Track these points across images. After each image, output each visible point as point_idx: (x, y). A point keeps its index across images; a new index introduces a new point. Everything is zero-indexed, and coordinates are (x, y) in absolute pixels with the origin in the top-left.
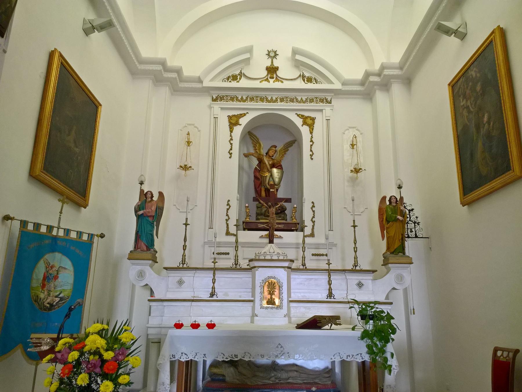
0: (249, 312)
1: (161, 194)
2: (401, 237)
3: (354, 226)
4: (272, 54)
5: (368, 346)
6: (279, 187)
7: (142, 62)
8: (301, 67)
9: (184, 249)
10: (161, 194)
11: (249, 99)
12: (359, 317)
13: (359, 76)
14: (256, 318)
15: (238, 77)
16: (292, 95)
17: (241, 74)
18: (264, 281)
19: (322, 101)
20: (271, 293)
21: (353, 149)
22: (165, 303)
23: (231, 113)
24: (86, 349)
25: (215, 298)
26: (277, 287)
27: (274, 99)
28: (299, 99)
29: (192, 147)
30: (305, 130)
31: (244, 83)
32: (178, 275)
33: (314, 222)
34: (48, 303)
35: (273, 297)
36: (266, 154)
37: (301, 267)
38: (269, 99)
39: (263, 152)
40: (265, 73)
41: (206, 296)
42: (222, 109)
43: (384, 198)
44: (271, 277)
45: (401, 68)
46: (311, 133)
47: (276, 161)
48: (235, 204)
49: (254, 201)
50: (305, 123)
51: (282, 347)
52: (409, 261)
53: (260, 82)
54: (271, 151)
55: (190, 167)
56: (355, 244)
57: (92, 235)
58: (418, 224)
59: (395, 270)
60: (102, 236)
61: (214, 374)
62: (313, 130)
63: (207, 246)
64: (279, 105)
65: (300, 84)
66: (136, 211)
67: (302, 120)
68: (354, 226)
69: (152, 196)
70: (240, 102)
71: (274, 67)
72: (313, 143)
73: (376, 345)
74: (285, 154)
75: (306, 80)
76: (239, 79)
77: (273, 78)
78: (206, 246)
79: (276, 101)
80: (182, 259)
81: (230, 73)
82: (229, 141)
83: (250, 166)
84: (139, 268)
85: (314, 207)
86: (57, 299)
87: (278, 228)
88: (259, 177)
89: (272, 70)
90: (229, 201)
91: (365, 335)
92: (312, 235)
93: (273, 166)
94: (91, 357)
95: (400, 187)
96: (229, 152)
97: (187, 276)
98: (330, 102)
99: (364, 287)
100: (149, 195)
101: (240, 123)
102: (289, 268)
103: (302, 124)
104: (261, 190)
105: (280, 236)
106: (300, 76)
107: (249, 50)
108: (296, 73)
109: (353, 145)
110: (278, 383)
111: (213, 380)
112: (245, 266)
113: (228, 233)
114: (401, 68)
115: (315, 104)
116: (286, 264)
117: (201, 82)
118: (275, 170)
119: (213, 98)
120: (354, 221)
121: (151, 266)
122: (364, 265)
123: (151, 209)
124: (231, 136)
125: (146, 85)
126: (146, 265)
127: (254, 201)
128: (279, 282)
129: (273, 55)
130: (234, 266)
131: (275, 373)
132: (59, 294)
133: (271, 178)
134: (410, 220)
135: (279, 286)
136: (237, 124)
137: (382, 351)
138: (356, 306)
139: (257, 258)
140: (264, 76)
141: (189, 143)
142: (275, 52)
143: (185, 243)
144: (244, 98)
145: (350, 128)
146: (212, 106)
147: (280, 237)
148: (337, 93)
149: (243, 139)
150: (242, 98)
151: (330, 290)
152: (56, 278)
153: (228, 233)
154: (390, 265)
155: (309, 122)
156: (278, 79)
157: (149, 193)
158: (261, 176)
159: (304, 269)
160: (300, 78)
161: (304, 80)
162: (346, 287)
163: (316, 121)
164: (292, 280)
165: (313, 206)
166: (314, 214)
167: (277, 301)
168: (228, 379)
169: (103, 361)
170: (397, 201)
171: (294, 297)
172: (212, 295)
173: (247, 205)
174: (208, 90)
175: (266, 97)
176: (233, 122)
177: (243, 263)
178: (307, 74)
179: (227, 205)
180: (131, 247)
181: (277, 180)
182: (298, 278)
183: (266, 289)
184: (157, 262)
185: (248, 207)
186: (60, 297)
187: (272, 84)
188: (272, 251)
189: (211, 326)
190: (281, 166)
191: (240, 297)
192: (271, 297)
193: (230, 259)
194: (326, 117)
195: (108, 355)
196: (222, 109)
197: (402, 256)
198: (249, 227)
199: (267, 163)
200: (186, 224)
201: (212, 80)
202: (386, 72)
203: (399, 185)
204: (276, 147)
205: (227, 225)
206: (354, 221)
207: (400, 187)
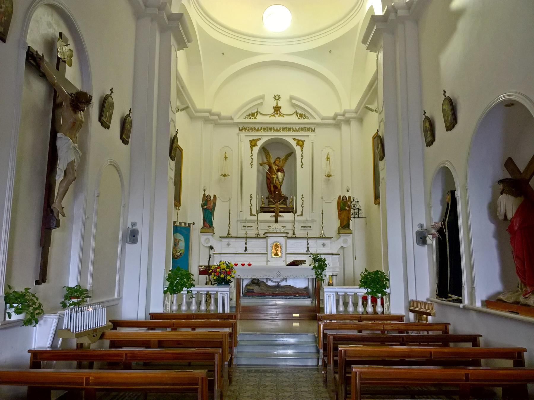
0: (265, 259)
1: (215, 196)
2: (347, 219)
3: (322, 213)
4: (277, 98)
5: (316, 272)
6: (282, 184)
7: (197, 111)
8: (296, 107)
9: (229, 226)
10: (215, 196)
11: (262, 129)
12: (313, 261)
13: (332, 114)
14: (268, 262)
15: (255, 114)
16: (290, 126)
17: (257, 112)
18: (272, 244)
19: (309, 130)
20: (276, 250)
21: (328, 160)
22: (222, 255)
23: (252, 138)
24: (221, 268)
25: (247, 252)
26: (280, 247)
27: (278, 129)
28: (294, 129)
29: (228, 160)
30: (298, 149)
31: (260, 119)
32: (228, 241)
33: (303, 207)
34: (176, 256)
35: (278, 252)
36: (274, 163)
37: (293, 236)
38: (275, 129)
39: (272, 161)
40: (273, 110)
41: (243, 252)
42: (246, 136)
43: (340, 197)
44: (276, 242)
45: (356, 113)
46: (302, 151)
47: (280, 167)
48: (254, 196)
49: (266, 199)
50: (298, 144)
51: (279, 273)
52: (350, 232)
53: (270, 117)
54: (277, 162)
55: (228, 175)
56: (322, 223)
57: (190, 224)
58: (361, 210)
59: (343, 237)
60: (194, 224)
61: (248, 289)
62: (303, 149)
63: (239, 223)
64: (282, 133)
65: (294, 119)
66: (202, 207)
67: (296, 142)
68: (322, 213)
69: (210, 198)
70: (257, 131)
71: (278, 107)
72: (303, 157)
73: (318, 272)
74: (286, 161)
75: (299, 115)
76: (256, 115)
77: (278, 114)
78: (239, 223)
79: (279, 130)
80: (229, 232)
81: (250, 112)
82: (251, 157)
83: (263, 169)
84: (206, 237)
85: (303, 198)
86: (179, 254)
87: (281, 211)
88: (269, 178)
89: (277, 109)
90: (251, 195)
91: (314, 267)
92: (302, 215)
93: (278, 171)
94: (223, 270)
95: (348, 191)
96: (251, 164)
97: (231, 241)
98: (314, 131)
99: (325, 246)
100: (209, 197)
101: (257, 145)
102: (287, 237)
103: (296, 145)
104: (271, 186)
105: (282, 216)
106: (295, 112)
107: (262, 97)
108: (292, 111)
109: (328, 158)
110: (280, 293)
111: (248, 292)
112: (262, 236)
113: (251, 214)
114: (356, 113)
115: (304, 132)
116: (284, 235)
117: (233, 119)
118: (279, 173)
119: (240, 129)
120: (322, 210)
121: (212, 236)
122: (326, 235)
123: (210, 205)
124: (252, 153)
125: (199, 125)
126: (209, 235)
127: (266, 199)
128: (280, 244)
129: (277, 98)
130: (257, 235)
131: (279, 289)
132: (180, 252)
133: (277, 179)
134: (356, 208)
135: (281, 247)
136: (255, 145)
137: (321, 274)
138: (312, 256)
139: (269, 232)
140: (272, 113)
141: (226, 158)
142: (279, 96)
143: (229, 224)
144: (260, 129)
145: (326, 147)
146: (239, 134)
147: (282, 216)
148: (318, 124)
149: (260, 152)
150: (258, 128)
151: (308, 247)
152: (178, 244)
153: (251, 214)
154: (340, 234)
155: (301, 143)
156: (281, 115)
157: (209, 196)
158: (271, 177)
159: (294, 237)
160: (295, 114)
161: (297, 116)
162: (316, 246)
163: (305, 143)
164: (287, 243)
165: (303, 197)
166: (303, 202)
167: (280, 254)
168: (255, 291)
169: (227, 272)
170: (346, 199)
171: (288, 252)
172: (245, 251)
173: (262, 197)
174: (237, 124)
175: (273, 127)
176: (253, 144)
177: (261, 233)
178: (299, 112)
179: (250, 197)
180: (202, 226)
181: (281, 180)
182: (290, 242)
183: (274, 248)
184: (214, 234)
185: (263, 198)
186: (180, 253)
187: (277, 119)
188: (277, 228)
189: (249, 265)
190: (283, 170)
191: (260, 252)
192: (276, 252)
193: (253, 229)
194: (311, 140)
195: (228, 270)
196: (246, 136)
197: (347, 229)
198: (263, 210)
199: (274, 169)
200: (230, 213)
201: (238, 118)
202: (347, 115)
203: (348, 190)
204: (280, 158)
205: (251, 209)
206: (322, 210)
207: (348, 191)
